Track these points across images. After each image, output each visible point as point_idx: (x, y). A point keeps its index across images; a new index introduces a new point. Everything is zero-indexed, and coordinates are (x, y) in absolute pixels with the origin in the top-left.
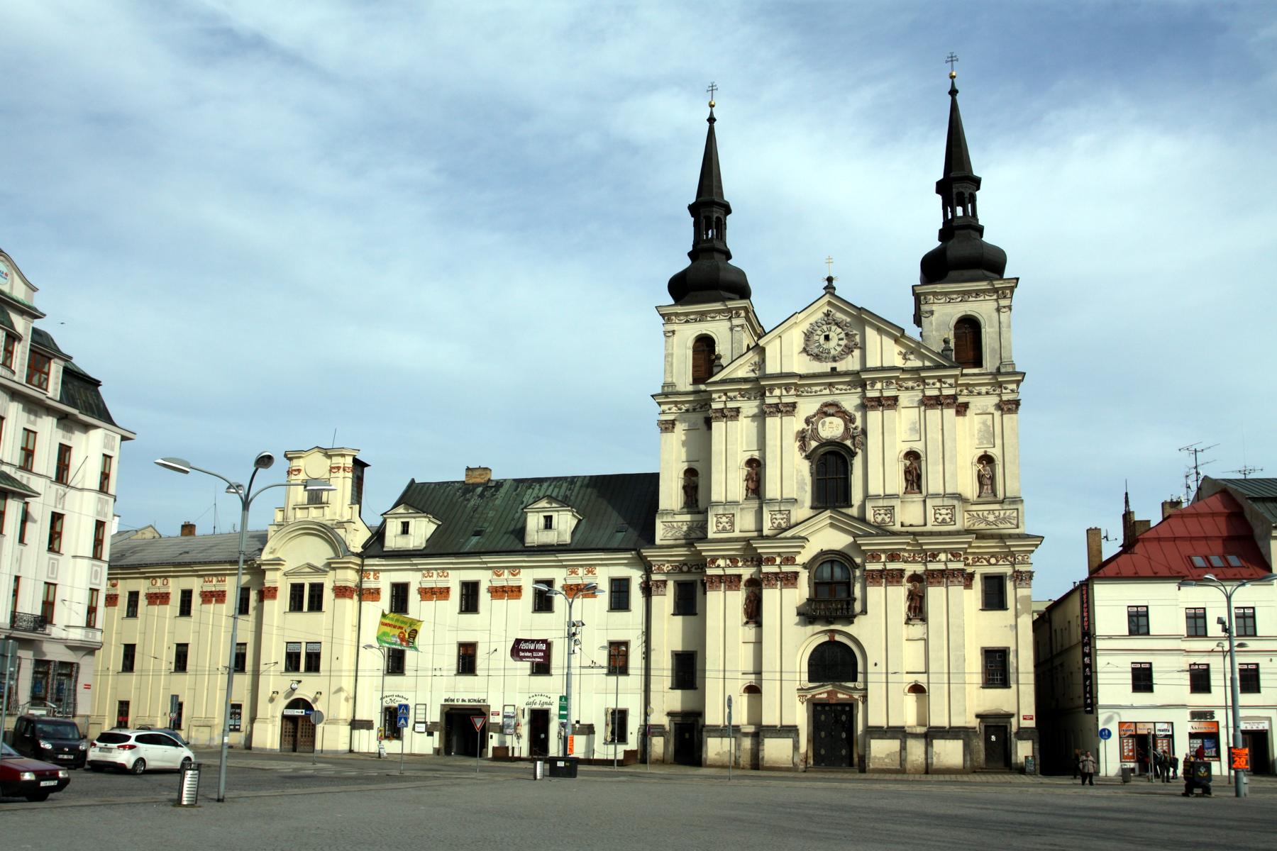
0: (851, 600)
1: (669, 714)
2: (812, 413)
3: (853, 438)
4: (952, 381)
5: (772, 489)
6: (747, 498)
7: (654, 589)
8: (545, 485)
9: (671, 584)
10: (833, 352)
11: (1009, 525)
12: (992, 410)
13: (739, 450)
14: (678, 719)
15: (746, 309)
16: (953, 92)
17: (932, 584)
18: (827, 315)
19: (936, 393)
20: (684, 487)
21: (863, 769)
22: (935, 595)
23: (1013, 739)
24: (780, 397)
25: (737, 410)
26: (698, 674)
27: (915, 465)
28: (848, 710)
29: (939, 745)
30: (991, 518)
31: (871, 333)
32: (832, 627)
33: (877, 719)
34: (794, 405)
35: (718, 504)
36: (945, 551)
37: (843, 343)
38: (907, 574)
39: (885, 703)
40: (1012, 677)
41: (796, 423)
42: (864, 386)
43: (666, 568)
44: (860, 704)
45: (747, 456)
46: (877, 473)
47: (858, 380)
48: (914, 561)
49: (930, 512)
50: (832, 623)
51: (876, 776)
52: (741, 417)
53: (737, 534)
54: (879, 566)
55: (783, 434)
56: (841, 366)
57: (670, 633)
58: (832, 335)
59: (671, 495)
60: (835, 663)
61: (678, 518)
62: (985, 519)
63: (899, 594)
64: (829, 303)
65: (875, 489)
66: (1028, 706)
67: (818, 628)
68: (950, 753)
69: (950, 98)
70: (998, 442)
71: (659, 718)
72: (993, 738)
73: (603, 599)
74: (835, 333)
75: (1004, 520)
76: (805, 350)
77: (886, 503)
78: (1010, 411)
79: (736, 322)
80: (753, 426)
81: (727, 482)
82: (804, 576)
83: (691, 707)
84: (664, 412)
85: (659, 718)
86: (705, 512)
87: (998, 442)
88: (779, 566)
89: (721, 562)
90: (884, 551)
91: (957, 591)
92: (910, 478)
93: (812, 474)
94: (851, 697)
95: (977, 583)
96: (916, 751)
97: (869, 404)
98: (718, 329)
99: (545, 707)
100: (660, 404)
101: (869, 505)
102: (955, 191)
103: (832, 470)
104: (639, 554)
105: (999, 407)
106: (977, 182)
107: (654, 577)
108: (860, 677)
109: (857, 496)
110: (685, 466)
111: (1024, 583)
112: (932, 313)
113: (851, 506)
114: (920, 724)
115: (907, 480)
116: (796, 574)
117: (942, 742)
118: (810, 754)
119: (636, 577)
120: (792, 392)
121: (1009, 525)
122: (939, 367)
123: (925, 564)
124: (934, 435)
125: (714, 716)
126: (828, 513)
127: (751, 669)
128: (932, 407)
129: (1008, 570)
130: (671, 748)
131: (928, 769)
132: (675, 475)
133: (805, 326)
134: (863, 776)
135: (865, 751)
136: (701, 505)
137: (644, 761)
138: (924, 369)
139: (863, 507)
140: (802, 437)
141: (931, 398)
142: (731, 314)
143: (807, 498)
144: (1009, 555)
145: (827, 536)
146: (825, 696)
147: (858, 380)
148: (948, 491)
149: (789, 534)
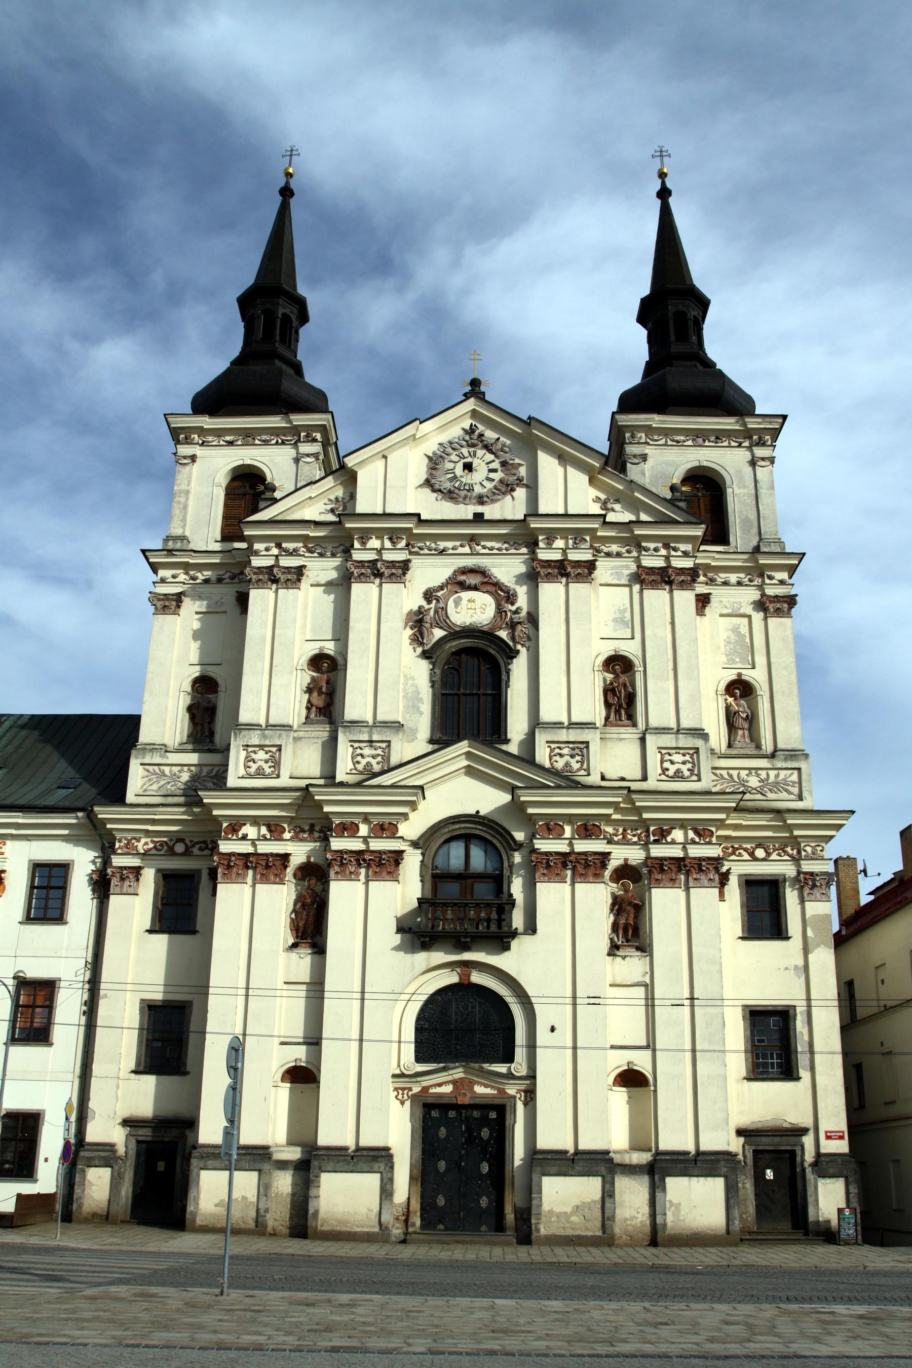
0: (506, 905)
1: (126, 1122)
2: (437, 583)
3: (512, 626)
4: (688, 547)
5: (356, 704)
6: (308, 720)
7: (114, 881)
9: (149, 876)
10: (478, 490)
11: (784, 795)
12: (749, 610)
13: (298, 639)
14: (146, 1133)
15: (323, 429)
16: (664, 194)
17: (659, 883)
18: (471, 431)
19: (660, 563)
20: (190, 709)
21: (525, 1236)
24: (379, 552)
25: (300, 571)
26: (192, 1038)
27: (623, 678)
28: (497, 1115)
29: (678, 1188)
30: (754, 782)
31: (547, 463)
32: (467, 956)
33: (553, 1135)
34: (405, 566)
36: (683, 825)
37: (497, 476)
38: (613, 864)
39: (569, 1101)
40: (803, 1060)
41: (407, 597)
42: (533, 545)
43: (143, 844)
44: (520, 1107)
45: (313, 649)
46: (556, 685)
47: (524, 535)
48: (625, 842)
50: (466, 948)
52: (305, 583)
53: (284, 781)
54: (561, 847)
55: (383, 620)
56: (491, 511)
57: (140, 962)
58: (476, 463)
60: (470, 1027)
61: (174, 758)
63: (596, 898)
64: (474, 414)
65: (552, 709)
66: (834, 1115)
67: (439, 957)
68: (699, 1203)
69: (279, 199)
70: (761, 660)
71: (105, 1129)
72: (769, 1175)
74: (482, 460)
75: (777, 786)
76: (428, 483)
77: (574, 735)
78: (779, 613)
79: (305, 448)
80: (327, 602)
81: (271, 690)
82: (412, 862)
83: (172, 1109)
84: (163, 581)
85: (105, 1129)
87: (761, 660)
88: (365, 840)
89: (250, 831)
90: (570, 819)
91: (704, 896)
92: (613, 700)
93: (433, 683)
94: (502, 1092)
95: (733, 888)
96: (632, 1198)
97: (543, 572)
98: (276, 462)
100: (154, 568)
101: (541, 739)
102: (671, 309)
103: (472, 683)
104: (91, 816)
105: (761, 605)
106: (703, 304)
107: (118, 861)
108: (520, 1053)
109: (517, 725)
110: (196, 672)
111: (817, 893)
112: (644, 458)
113: (507, 741)
114: (635, 1147)
115: (608, 705)
116: (397, 857)
117: (683, 1181)
118: (416, 1205)
119: (83, 861)
120: (403, 544)
123: (646, 846)
126: (463, 746)
128: (654, 585)
129: (788, 870)
130: (126, 1190)
131: (656, 1236)
132: (174, 685)
133: (431, 446)
135: (530, 1199)
137: (68, 1217)
139: (530, 742)
142: (294, 436)
143: (422, 724)
144: (790, 845)
145: (459, 790)
146: (448, 1089)
147: (524, 535)
148: (685, 724)
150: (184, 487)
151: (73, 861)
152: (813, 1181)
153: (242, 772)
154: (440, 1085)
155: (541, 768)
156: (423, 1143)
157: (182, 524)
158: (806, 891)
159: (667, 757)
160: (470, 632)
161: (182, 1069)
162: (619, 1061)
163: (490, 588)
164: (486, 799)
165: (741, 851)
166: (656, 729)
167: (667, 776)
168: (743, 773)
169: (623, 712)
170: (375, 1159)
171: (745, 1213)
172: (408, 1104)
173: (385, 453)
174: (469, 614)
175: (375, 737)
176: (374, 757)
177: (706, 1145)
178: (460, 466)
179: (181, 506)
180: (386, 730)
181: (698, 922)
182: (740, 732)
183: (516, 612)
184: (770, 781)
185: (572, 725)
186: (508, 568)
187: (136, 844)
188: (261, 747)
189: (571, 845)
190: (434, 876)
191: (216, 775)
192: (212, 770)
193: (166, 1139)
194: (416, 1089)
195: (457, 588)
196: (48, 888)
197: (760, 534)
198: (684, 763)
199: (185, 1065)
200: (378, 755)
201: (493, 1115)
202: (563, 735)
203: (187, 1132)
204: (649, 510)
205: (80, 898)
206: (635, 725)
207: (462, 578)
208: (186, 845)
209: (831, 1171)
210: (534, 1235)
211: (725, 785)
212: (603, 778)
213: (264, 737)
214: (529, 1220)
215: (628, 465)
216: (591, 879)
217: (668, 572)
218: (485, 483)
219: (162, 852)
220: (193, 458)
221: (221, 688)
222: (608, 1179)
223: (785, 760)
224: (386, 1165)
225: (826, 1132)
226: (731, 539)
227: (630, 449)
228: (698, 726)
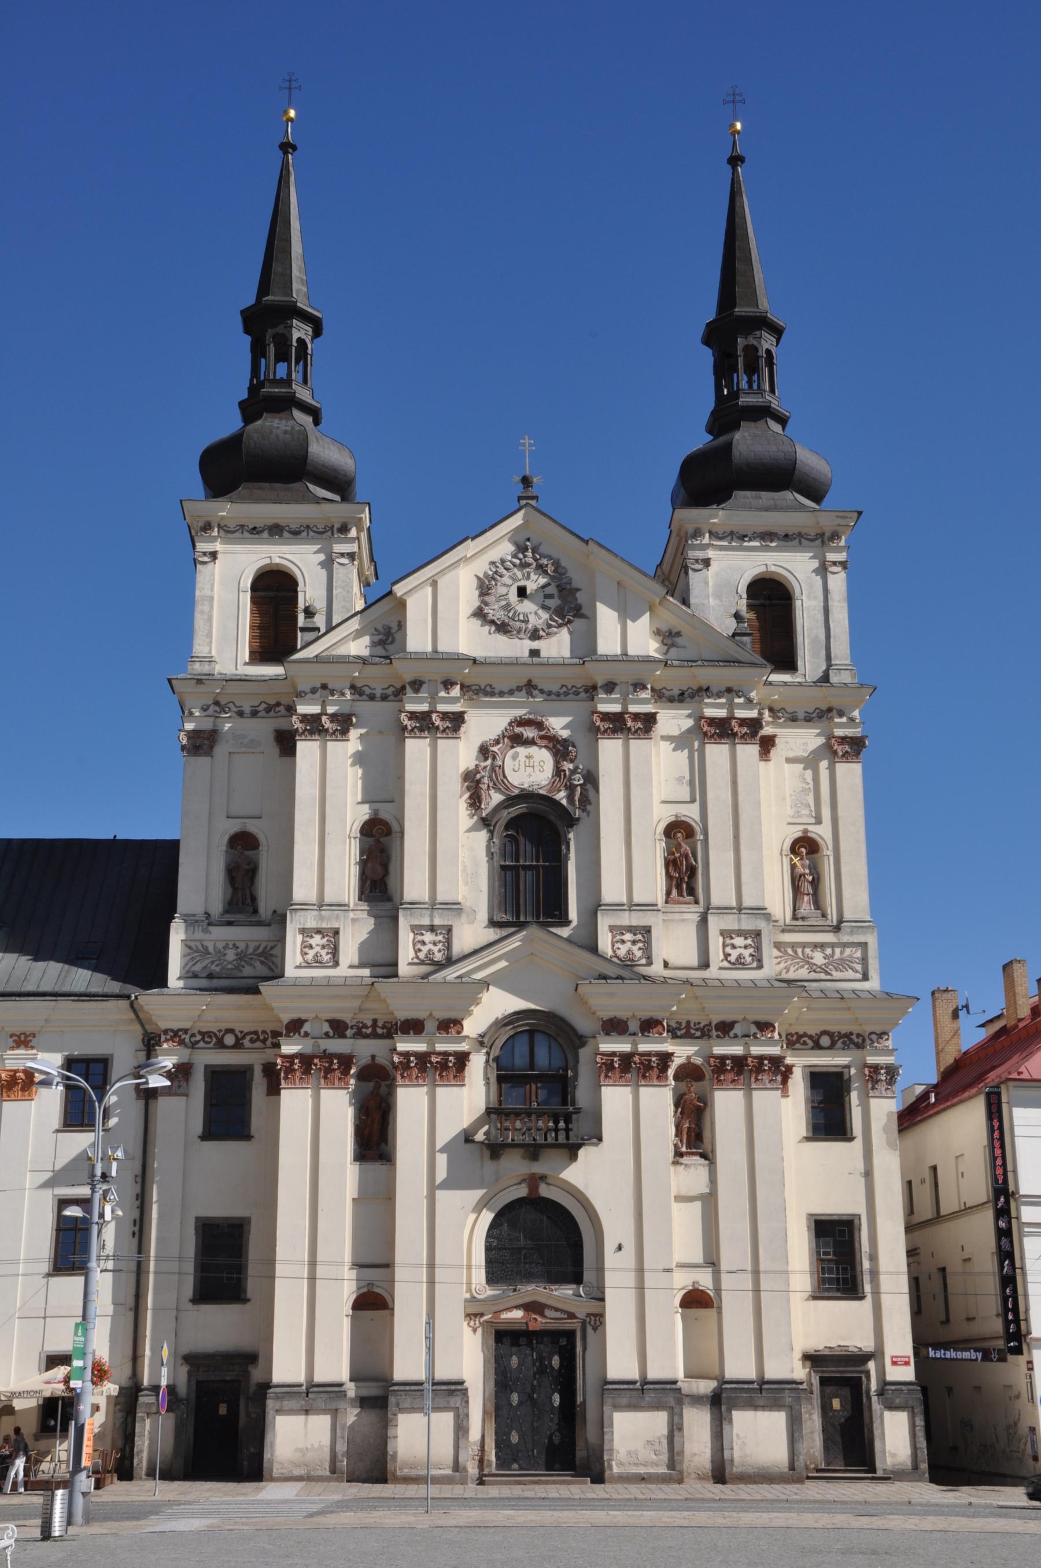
5: (414, 884)
10: (534, 621)
11: (850, 974)
22: (727, 1104)
30: (818, 958)
33: (621, 1364)
34: (457, 720)
35: (304, 906)
41: (461, 754)
46: (621, 862)
51: (635, 1491)
59: (199, 883)
60: (541, 1240)
62: (807, 961)
63: (659, 1101)
65: (612, 890)
66: (899, 1340)
70: (826, 813)
73: (50, 1101)
75: (843, 964)
76: (479, 614)
81: (322, 866)
82: (477, 1063)
86: (279, 920)
87: (826, 813)
91: (764, 1098)
95: (798, 1083)
101: (604, 922)
103: (537, 850)
112: (707, 563)
116: (462, 1059)
121: (850, 974)
125: (286, 1366)
127: (699, 1258)
134: (598, 1491)
135: (602, 1434)
136: (265, 906)
140: (472, 781)
141: (712, 721)
148: (747, 902)
150: (207, 593)
151: (112, 1055)
152: (879, 1412)
153: (299, 959)
154: (509, 1309)
155: (603, 957)
156: (496, 1374)
157: (208, 640)
159: (728, 941)
160: (526, 796)
161: (242, 1297)
162: (683, 1281)
165: (806, 1039)
166: (719, 908)
167: (729, 962)
169: (684, 886)
170: (452, 1393)
171: (813, 1448)
172: (480, 1331)
173: (435, 578)
174: (527, 773)
176: (435, 944)
177: (772, 1372)
178: (514, 591)
179: (205, 617)
180: (446, 912)
182: (806, 898)
184: (836, 957)
185: (632, 906)
187: (183, 1036)
188: (319, 931)
191: (263, 952)
192: (259, 947)
193: (228, 1378)
197: (828, 657)
198: (746, 947)
199: (245, 1291)
200: (440, 942)
201: (563, 1342)
202: (626, 919)
203: (251, 1368)
206: (697, 902)
207: (518, 730)
208: (236, 1036)
210: (607, 1473)
211: (789, 962)
212: (666, 965)
213: (322, 918)
214: (602, 1457)
215: (690, 572)
216: (656, 1082)
217: (730, 724)
219: (211, 1045)
220: (214, 555)
221: (263, 848)
222: (677, 1410)
223: (852, 933)
224: (462, 1399)
225: (892, 1357)
226: (800, 663)
227: (692, 554)
228: (760, 904)
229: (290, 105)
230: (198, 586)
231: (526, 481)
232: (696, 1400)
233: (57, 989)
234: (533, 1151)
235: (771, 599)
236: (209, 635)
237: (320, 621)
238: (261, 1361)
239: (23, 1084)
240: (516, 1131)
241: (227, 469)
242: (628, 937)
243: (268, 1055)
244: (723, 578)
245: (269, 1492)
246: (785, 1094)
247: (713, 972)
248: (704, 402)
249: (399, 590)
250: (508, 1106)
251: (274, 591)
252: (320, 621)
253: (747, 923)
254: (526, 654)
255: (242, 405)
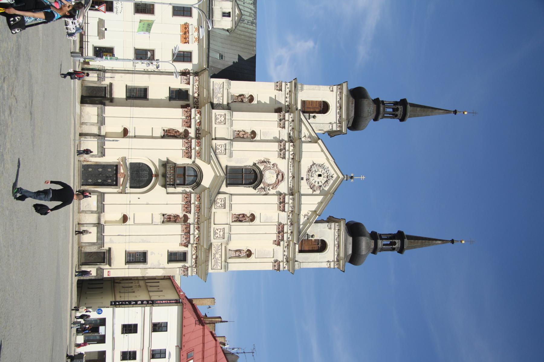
0: (174, 185)
5: (237, 145)
8: (252, 7)
10: (311, 179)
23: (97, 266)
28: (115, 183)
30: (218, 256)
33: (108, 198)
37: (316, 184)
39: (118, 200)
41: (274, 158)
46: (243, 199)
49: (221, 227)
53: (214, 126)
54: (192, 201)
56: (304, 183)
60: (140, 176)
63: (179, 211)
66: (114, 274)
70: (258, 260)
74: (323, 179)
76: (314, 164)
81: (243, 121)
82: (189, 161)
87: (258, 260)
92: (241, 216)
95: (183, 249)
99: (115, 10)
103: (250, 177)
112: (330, 228)
113: (227, 186)
118: (89, 163)
122: (299, 232)
124: (263, 229)
133: (327, 165)
138: (299, 225)
143: (234, 163)
146: (122, 171)
149: (212, 154)
155: (216, 196)
158: (183, 269)
160: (262, 176)
162: (130, 215)
163: (277, 182)
164: (206, 182)
168: (220, 253)
170: (102, 153)
175: (227, 151)
178: (320, 173)
181: (172, 238)
183: (269, 189)
186: (283, 188)
188: (225, 119)
189: (193, 203)
190: (185, 167)
194: (122, 163)
195: (277, 173)
196: (184, 56)
202: (227, 202)
204: (303, 228)
205: (182, 66)
207: (281, 174)
209: (99, 272)
213: (228, 120)
218: (314, 181)
227: (333, 224)
229: (468, 113)
230: (323, 86)
231: (352, 177)
232: (99, 219)
233: (210, 49)
234: (164, 176)
235: (322, 246)
236: (309, 89)
237: (312, 119)
238: (111, 104)
239: (185, 40)
240: (170, 172)
241: (357, 95)
242: (223, 203)
243: (192, 105)
244: (327, 233)
245: (78, 105)
246: (181, 244)
247: (213, 226)
248: (380, 231)
249: (320, 141)
250: (177, 169)
251: (324, 108)
252: (312, 119)
253: (226, 236)
254: (302, 176)
255: (378, 99)
